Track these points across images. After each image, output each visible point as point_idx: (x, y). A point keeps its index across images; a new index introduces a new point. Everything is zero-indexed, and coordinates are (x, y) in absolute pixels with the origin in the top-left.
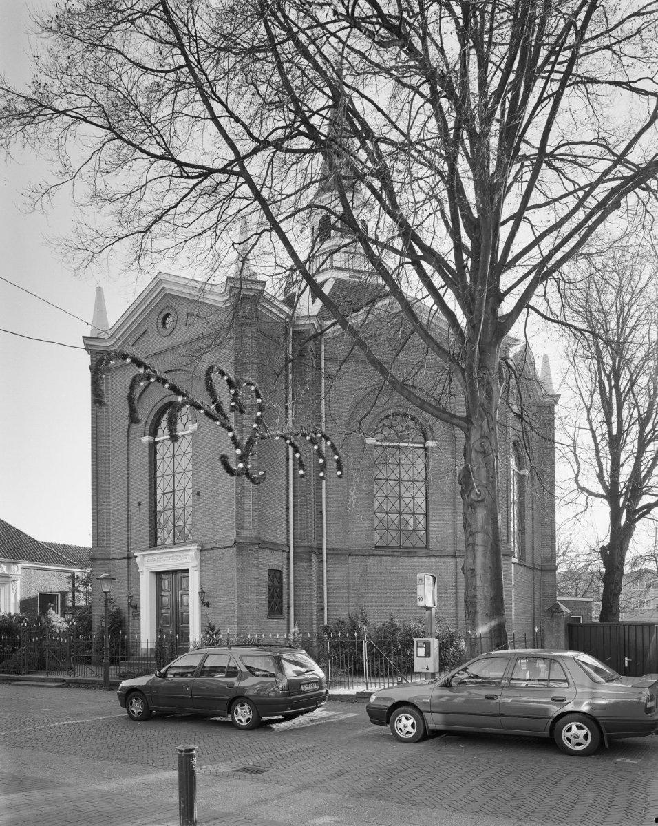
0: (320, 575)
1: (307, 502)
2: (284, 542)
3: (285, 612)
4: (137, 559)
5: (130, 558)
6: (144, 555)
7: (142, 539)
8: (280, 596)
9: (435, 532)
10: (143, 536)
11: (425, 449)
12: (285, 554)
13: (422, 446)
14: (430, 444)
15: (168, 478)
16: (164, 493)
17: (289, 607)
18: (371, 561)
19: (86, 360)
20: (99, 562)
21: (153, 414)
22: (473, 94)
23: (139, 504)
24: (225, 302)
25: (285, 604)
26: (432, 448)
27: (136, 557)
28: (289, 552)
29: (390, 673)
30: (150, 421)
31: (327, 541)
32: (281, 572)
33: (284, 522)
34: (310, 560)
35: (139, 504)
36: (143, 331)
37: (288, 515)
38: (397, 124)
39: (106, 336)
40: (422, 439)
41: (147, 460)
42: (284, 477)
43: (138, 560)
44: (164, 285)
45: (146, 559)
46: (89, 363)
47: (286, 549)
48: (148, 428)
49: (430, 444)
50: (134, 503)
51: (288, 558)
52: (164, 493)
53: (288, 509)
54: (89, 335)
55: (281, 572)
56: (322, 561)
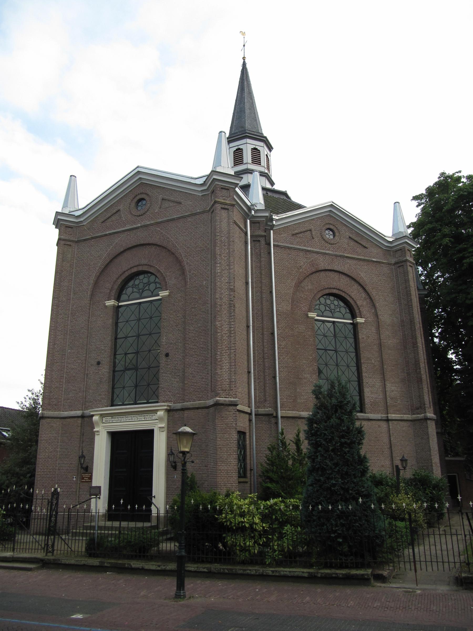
14: (359, 320)
49: (359, 320)
51: (250, 420)
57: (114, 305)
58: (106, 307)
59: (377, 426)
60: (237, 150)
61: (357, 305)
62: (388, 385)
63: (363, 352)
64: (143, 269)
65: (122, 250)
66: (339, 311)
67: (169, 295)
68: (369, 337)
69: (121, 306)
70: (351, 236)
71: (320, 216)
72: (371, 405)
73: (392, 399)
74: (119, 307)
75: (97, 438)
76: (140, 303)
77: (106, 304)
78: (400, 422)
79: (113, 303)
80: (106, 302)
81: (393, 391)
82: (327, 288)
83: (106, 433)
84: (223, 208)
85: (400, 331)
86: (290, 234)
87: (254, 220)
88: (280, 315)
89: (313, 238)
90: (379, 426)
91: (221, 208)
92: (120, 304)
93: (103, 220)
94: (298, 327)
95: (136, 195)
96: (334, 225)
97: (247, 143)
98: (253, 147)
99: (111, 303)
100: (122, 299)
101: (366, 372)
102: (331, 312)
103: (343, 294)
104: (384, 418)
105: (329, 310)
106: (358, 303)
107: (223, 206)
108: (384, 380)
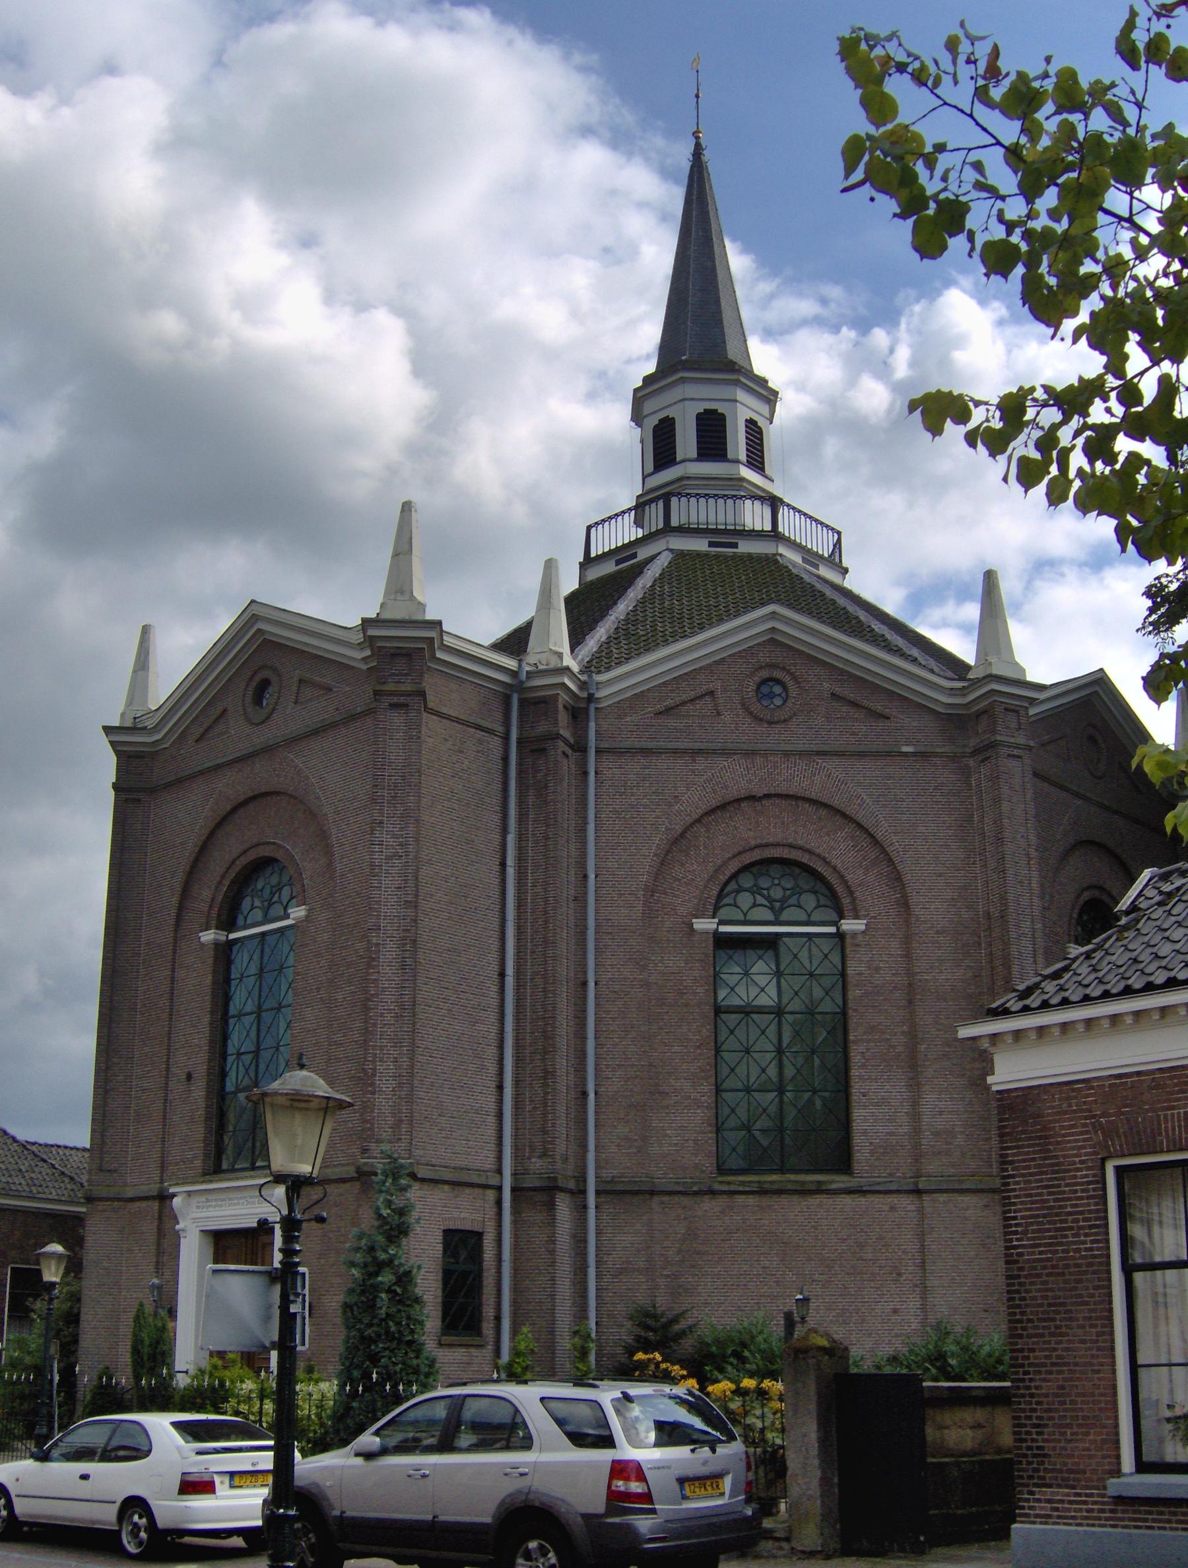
0: (580, 1241)
1: (546, 1072)
2: (489, 1163)
3: (488, 1328)
4: (175, 1200)
5: (164, 1198)
6: (189, 1193)
7: (189, 1154)
8: (475, 1289)
9: (865, 1132)
10: (191, 1149)
11: (840, 936)
12: (491, 1195)
13: (832, 930)
14: (848, 925)
15: (248, 1020)
16: (239, 1054)
17: (498, 1318)
18: (708, 1205)
19: (107, 766)
20: (101, 1205)
21: (227, 883)
22: (668, 542)
23: (189, 1077)
24: (364, 659)
25: (489, 1312)
26: (854, 934)
27: (174, 1195)
28: (499, 1189)
29: (1012, 1299)
30: (220, 897)
31: (597, 1161)
32: (479, 1235)
33: (491, 1120)
34: (551, 1206)
35: (189, 1077)
36: (218, 712)
37: (500, 1101)
38: (264, 1014)
39: (150, 724)
40: (835, 917)
41: (209, 980)
42: (493, 1017)
43: (177, 1202)
44: (261, 626)
45: (194, 1201)
46: (113, 778)
47: (494, 1181)
48: (214, 913)
49: (848, 925)
50: (179, 1072)
51: (499, 1203)
52: (239, 1054)
53: (500, 1087)
54: (116, 723)
55: (479, 1235)
56: (585, 1207)
57: (215, 940)
58: (203, 945)
59: (886, 1208)
60: (662, 421)
61: (846, 882)
62: (930, 1100)
63: (855, 1010)
64: (267, 854)
65: (229, 808)
66: (796, 903)
67: (307, 916)
68: (878, 969)
69: (236, 940)
70: (838, 690)
71: (745, 647)
72: (872, 1153)
73: (936, 1134)
74: (231, 944)
75: (184, 1243)
76: (263, 934)
77: (202, 939)
78: (956, 1195)
79: (212, 936)
80: (200, 934)
81: (941, 1113)
82: (757, 847)
83: (198, 1232)
84: (394, 706)
85: (980, 944)
86: (650, 712)
87: (534, 695)
88: (610, 933)
89: (719, 714)
90: (893, 1208)
91: (391, 705)
92: (232, 936)
93: (198, 735)
94: (661, 961)
95: (255, 673)
96: (784, 669)
97: (684, 400)
98: (701, 407)
99: (208, 936)
100: (240, 921)
101: (863, 1066)
102: (772, 908)
103: (805, 859)
104: (905, 1188)
105: (765, 903)
106: (849, 877)
107: (395, 700)
108: (915, 1084)
